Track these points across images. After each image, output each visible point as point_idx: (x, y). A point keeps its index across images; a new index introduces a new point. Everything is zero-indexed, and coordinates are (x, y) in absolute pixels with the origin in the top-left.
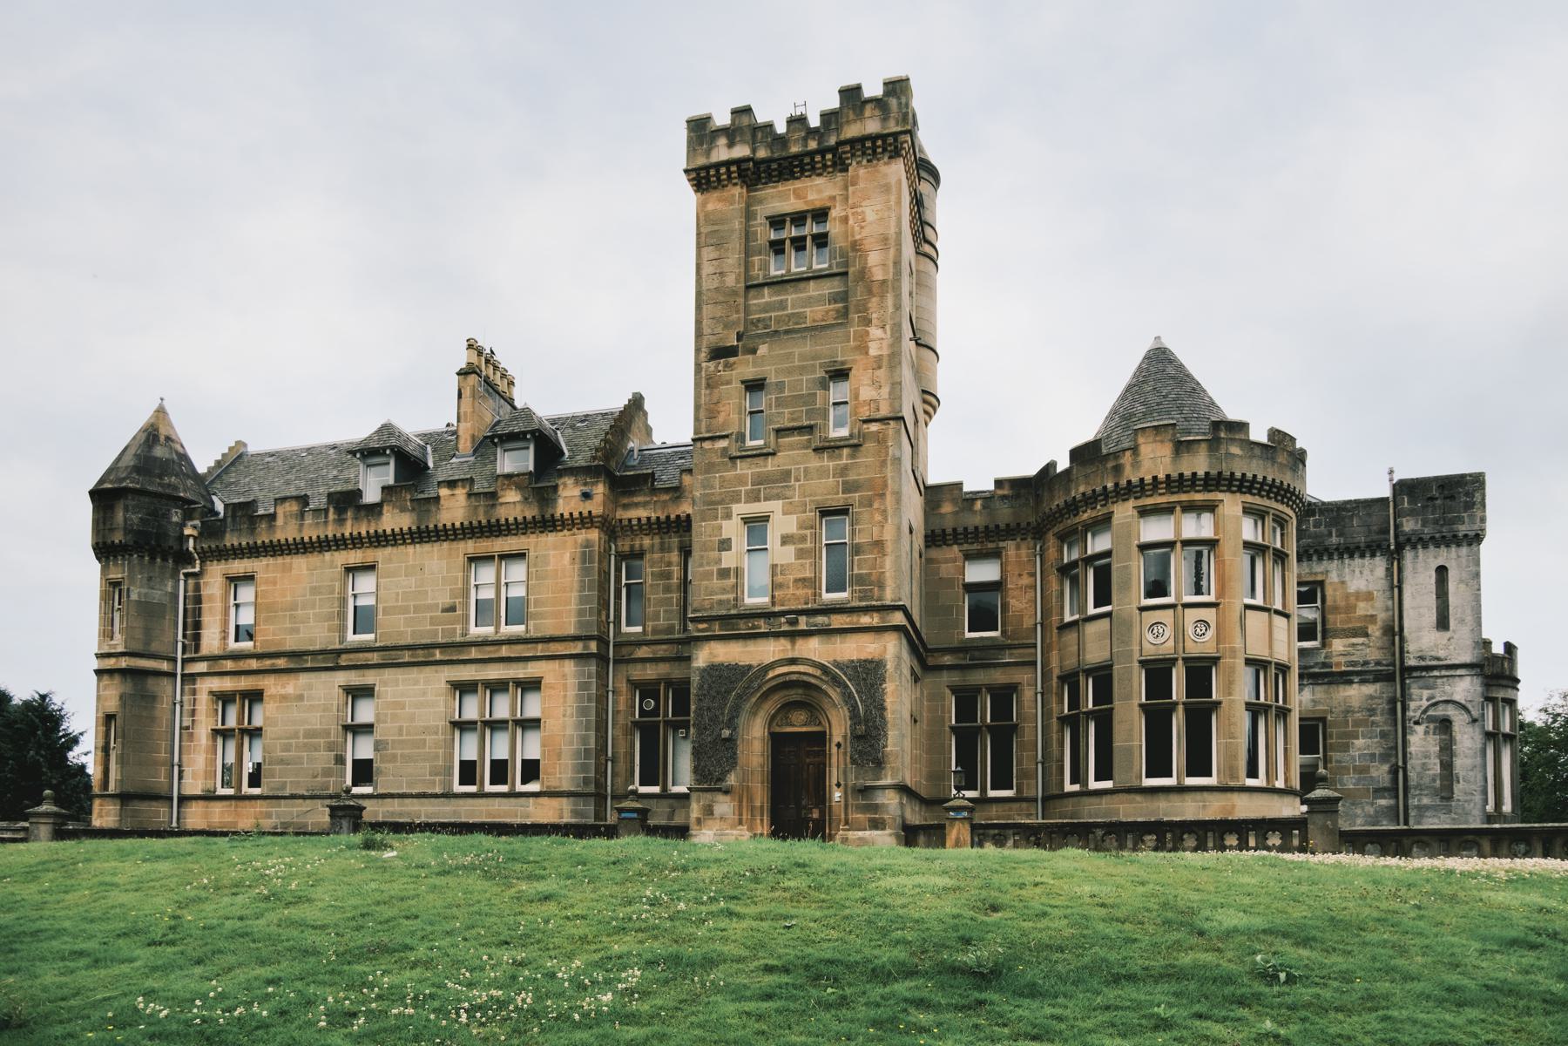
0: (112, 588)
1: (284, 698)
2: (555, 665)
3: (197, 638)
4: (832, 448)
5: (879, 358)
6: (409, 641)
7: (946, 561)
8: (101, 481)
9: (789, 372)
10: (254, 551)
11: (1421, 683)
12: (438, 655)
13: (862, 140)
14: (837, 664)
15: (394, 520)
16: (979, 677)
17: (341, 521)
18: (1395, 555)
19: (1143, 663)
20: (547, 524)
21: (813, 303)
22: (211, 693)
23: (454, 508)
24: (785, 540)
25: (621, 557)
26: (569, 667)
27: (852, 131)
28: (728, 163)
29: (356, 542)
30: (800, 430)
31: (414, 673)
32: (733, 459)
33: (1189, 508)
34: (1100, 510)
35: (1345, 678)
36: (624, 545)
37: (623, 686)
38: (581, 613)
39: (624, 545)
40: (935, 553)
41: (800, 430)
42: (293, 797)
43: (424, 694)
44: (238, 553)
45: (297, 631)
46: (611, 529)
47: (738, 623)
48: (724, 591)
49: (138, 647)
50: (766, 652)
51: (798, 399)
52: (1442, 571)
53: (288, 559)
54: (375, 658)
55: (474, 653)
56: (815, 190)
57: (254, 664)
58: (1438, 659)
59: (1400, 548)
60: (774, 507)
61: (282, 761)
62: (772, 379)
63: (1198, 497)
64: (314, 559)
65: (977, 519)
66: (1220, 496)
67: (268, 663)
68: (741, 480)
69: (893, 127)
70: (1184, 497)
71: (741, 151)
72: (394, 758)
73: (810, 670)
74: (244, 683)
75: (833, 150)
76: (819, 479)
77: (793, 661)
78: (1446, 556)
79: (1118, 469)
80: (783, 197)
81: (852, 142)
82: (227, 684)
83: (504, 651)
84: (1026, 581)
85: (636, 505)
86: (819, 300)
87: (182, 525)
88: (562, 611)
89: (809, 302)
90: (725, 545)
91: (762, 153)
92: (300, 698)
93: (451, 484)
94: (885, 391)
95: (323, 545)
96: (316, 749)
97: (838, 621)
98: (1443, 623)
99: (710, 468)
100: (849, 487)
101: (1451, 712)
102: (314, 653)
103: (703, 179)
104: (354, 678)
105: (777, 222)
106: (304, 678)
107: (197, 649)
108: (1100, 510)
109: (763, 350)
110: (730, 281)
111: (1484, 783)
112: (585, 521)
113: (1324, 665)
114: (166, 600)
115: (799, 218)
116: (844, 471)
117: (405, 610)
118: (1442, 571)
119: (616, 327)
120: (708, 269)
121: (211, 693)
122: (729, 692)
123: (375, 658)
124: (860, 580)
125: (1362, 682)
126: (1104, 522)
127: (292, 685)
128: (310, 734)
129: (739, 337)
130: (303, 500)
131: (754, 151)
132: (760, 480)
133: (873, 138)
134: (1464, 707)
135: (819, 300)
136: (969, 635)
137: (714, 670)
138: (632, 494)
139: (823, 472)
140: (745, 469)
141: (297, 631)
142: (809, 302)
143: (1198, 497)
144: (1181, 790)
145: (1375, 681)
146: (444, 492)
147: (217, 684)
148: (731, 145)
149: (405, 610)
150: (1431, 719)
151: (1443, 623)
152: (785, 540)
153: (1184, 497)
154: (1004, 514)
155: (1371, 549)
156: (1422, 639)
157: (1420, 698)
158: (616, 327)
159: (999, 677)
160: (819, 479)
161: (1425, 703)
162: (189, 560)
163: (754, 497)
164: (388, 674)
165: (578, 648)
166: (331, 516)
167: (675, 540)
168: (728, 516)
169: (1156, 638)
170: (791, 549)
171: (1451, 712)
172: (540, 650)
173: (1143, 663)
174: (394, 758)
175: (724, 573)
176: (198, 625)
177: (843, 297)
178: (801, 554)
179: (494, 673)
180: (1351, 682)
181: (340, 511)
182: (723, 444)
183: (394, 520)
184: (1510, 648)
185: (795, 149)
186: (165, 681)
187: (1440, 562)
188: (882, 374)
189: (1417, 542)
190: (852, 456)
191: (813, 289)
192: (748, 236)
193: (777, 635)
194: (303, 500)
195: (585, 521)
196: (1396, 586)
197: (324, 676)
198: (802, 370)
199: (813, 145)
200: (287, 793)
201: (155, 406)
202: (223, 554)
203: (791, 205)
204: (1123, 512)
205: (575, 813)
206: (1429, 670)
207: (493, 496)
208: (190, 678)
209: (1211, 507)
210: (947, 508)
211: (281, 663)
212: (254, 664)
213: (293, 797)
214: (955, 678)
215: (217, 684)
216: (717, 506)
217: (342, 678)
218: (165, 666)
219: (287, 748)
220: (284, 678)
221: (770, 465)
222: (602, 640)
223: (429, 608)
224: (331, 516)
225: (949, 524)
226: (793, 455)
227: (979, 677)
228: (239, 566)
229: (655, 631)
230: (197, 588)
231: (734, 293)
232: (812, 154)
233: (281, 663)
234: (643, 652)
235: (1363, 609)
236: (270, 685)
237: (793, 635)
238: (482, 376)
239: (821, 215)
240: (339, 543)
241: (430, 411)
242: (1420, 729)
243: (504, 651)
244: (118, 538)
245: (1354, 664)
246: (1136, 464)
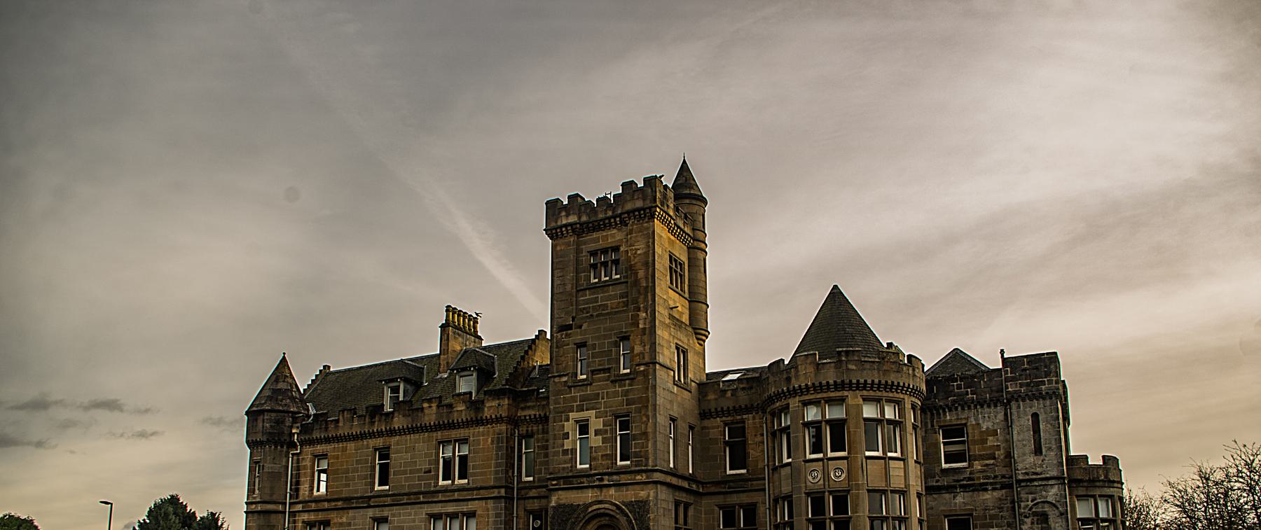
0: (254, 464)
1: (341, 524)
3: (297, 490)
4: (620, 379)
5: (644, 329)
7: (714, 428)
8: (252, 406)
9: (598, 338)
10: (327, 440)
11: (1027, 490)
13: (634, 211)
14: (623, 503)
15: (399, 422)
16: (734, 499)
17: (372, 423)
18: (1007, 405)
19: (808, 494)
20: (479, 422)
22: (303, 522)
23: (431, 414)
24: (597, 433)
25: (521, 437)
26: (491, 504)
27: (629, 206)
28: (566, 226)
29: (380, 434)
30: (604, 370)
31: (409, 509)
32: (570, 387)
33: (830, 401)
34: (784, 402)
35: (983, 488)
36: (523, 429)
37: (522, 513)
38: (497, 472)
39: (523, 429)
40: (706, 423)
41: (604, 370)
44: (319, 441)
45: (348, 485)
46: (514, 421)
47: (573, 480)
48: (565, 462)
49: (267, 498)
50: (589, 496)
51: (601, 354)
52: (1035, 416)
54: (389, 500)
55: (440, 497)
56: (614, 236)
57: (326, 505)
58: (1037, 474)
59: (1009, 402)
63: (832, 395)
65: (726, 403)
66: (846, 393)
68: (574, 399)
69: (648, 204)
70: (825, 395)
71: (573, 219)
73: (607, 506)
74: (321, 516)
75: (620, 216)
76: (614, 397)
77: (600, 502)
78: (1037, 406)
79: (788, 379)
81: (628, 212)
82: (312, 517)
83: (456, 496)
84: (759, 439)
85: (529, 408)
86: (615, 297)
87: (291, 427)
88: (486, 471)
90: (566, 436)
91: (584, 218)
92: (349, 524)
93: (430, 401)
94: (647, 347)
97: (624, 479)
98: (1038, 451)
99: (559, 393)
101: (1047, 508)
103: (552, 232)
104: (377, 513)
105: (593, 253)
106: (351, 513)
108: (784, 402)
110: (568, 287)
112: (499, 420)
113: (970, 479)
114: (282, 470)
115: (605, 251)
116: (626, 393)
118: (1035, 416)
119: (517, 304)
120: (557, 282)
121: (303, 522)
122: (567, 520)
123: (389, 500)
124: (637, 455)
125: (994, 489)
126: (786, 408)
129: (573, 319)
130: (354, 411)
131: (580, 218)
132: (583, 399)
133: (639, 210)
134: (1054, 505)
135: (615, 297)
136: (729, 472)
137: (559, 506)
138: (526, 401)
139: (616, 394)
143: (832, 395)
145: (1002, 488)
146: (426, 405)
147: (305, 517)
148: (567, 216)
149: (405, 472)
150: (1035, 514)
151: (1038, 451)
152: (597, 433)
153: (825, 395)
154: (743, 398)
155: (995, 402)
156: (1026, 461)
157: (1027, 502)
158: (517, 304)
159: (745, 498)
160: (614, 397)
161: (1030, 504)
162: (294, 446)
163: (581, 409)
165: (495, 493)
166: (367, 420)
168: (568, 420)
169: (814, 479)
171: (1047, 508)
172: (475, 495)
173: (808, 494)
175: (565, 452)
176: (298, 483)
178: (604, 440)
179: (451, 508)
180: (986, 490)
181: (372, 417)
182: (565, 379)
183: (399, 422)
184: (1110, 461)
185: (601, 216)
186: (280, 516)
187: (1034, 410)
188: (646, 338)
189: (1015, 397)
190: (630, 385)
191: (612, 291)
192: (577, 261)
193: (593, 487)
194: (354, 411)
195: (499, 420)
196: (1008, 423)
198: (605, 337)
199: (610, 213)
202: (311, 442)
203: (601, 244)
204: (794, 403)
206: (1033, 481)
207: (450, 406)
208: (293, 514)
209: (841, 401)
210: (711, 397)
212: (326, 505)
214: (720, 500)
215: (305, 517)
216: (563, 413)
217: (371, 513)
218: (280, 508)
222: (509, 489)
223: (419, 471)
224: (367, 420)
225: (713, 406)
227: (734, 499)
228: (320, 448)
229: (539, 480)
231: (571, 294)
232: (609, 218)
234: (533, 493)
235: (991, 441)
236: (333, 516)
237: (601, 487)
238: (458, 324)
239: (616, 249)
240: (372, 435)
241: (426, 343)
242: (1028, 521)
244: (259, 437)
245: (988, 477)
246: (797, 376)
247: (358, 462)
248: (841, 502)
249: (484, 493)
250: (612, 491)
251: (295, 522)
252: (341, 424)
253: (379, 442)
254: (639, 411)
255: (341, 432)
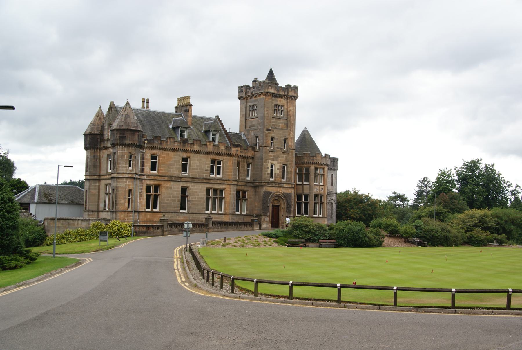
1: (167, 187)
2: (228, 186)
6: (198, 177)
10: (160, 149)
12: (204, 181)
15: (196, 148)
21: (281, 123)
26: (232, 187)
29: (187, 151)
31: (199, 185)
42: (169, 213)
43: (201, 190)
44: (156, 148)
45: (170, 171)
53: (168, 152)
55: (212, 181)
57: (159, 178)
60: (275, 162)
61: (166, 203)
62: (276, 137)
64: (175, 153)
67: (163, 178)
68: (271, 156)
72: (194, 204)
79: (313, 159)
80: (277, 101)
89: (281, 123)
92: (171, 188)
95: (178, 150)
96: (175, 201)
99: (266, 152)
100: (287, 161)
102: (175, 177)
106: (172, 183)
107: (143, 172)
109: (275, 131)
111: (323, 218)
115: (279, 106)
116: (286, 157)
117: (197, 169)
123: (190, 180)
124: (289, 178)
127: (169, 185)
128: (173, 197)
140: (271, 154)
141: (170, 171)
142: (281, 123)
144: (218, 214)
146: (208, 144)
149: (197, 169)
163: (273, 160)
164: (193, 184)
167: (246, 160)
170: (278, 171)
172: (226, 182)
174: (194, 204)
177: (287, 124)
191: (282, 121)
197: (177, 183)
200: (168, 211)
201: (126, 102)
203: (279, 103)
205: (232, 218)
211: (166, 178)
213: (169, 213)
219: (168, 200)
220: (167, 182)
221: (275, 154)
226: (279, 153)
230: (143, 155)
233: (166, 178)
239: (282, 106)
241: (165, 105)
243: (218, 182)
247: (175, 161)
248: (306, 197)
249: (229, 182)
250: (282, 189)
251: (142, 183)
252: (169, 143)
253: (185, 155)
254: (290, 164)
255: (169, 147)
